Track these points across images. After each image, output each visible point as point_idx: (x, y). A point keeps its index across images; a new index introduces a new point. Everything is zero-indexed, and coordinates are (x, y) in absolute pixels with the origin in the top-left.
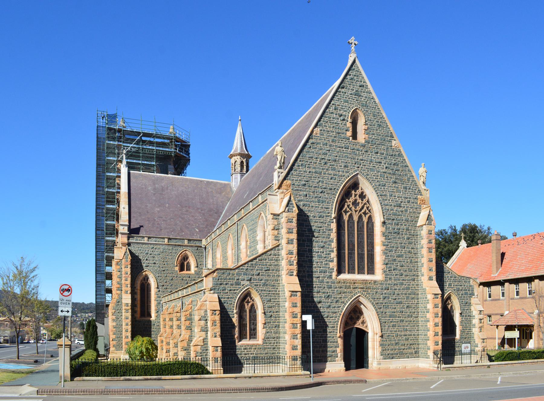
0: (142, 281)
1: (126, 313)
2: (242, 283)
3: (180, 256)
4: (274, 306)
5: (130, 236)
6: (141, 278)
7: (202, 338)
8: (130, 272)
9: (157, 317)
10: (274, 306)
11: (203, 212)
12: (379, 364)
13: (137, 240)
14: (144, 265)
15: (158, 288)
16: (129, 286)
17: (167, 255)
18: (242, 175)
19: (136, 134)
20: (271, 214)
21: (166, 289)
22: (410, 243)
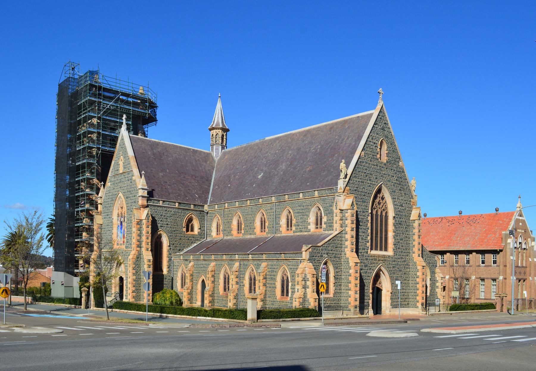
0: (156, 239)
2: (324, 255)
4: (339, 272)
6: (156, 237)
7: (303, 293)
10: (339, 272)
11: (196, 178)
12: (390, 311)
13: (154, 203)
14: (159, 225)
15: (169, 246)
16: (150, 244)
19: (115, 92)
20: (339, 209)
22: (407, 231)
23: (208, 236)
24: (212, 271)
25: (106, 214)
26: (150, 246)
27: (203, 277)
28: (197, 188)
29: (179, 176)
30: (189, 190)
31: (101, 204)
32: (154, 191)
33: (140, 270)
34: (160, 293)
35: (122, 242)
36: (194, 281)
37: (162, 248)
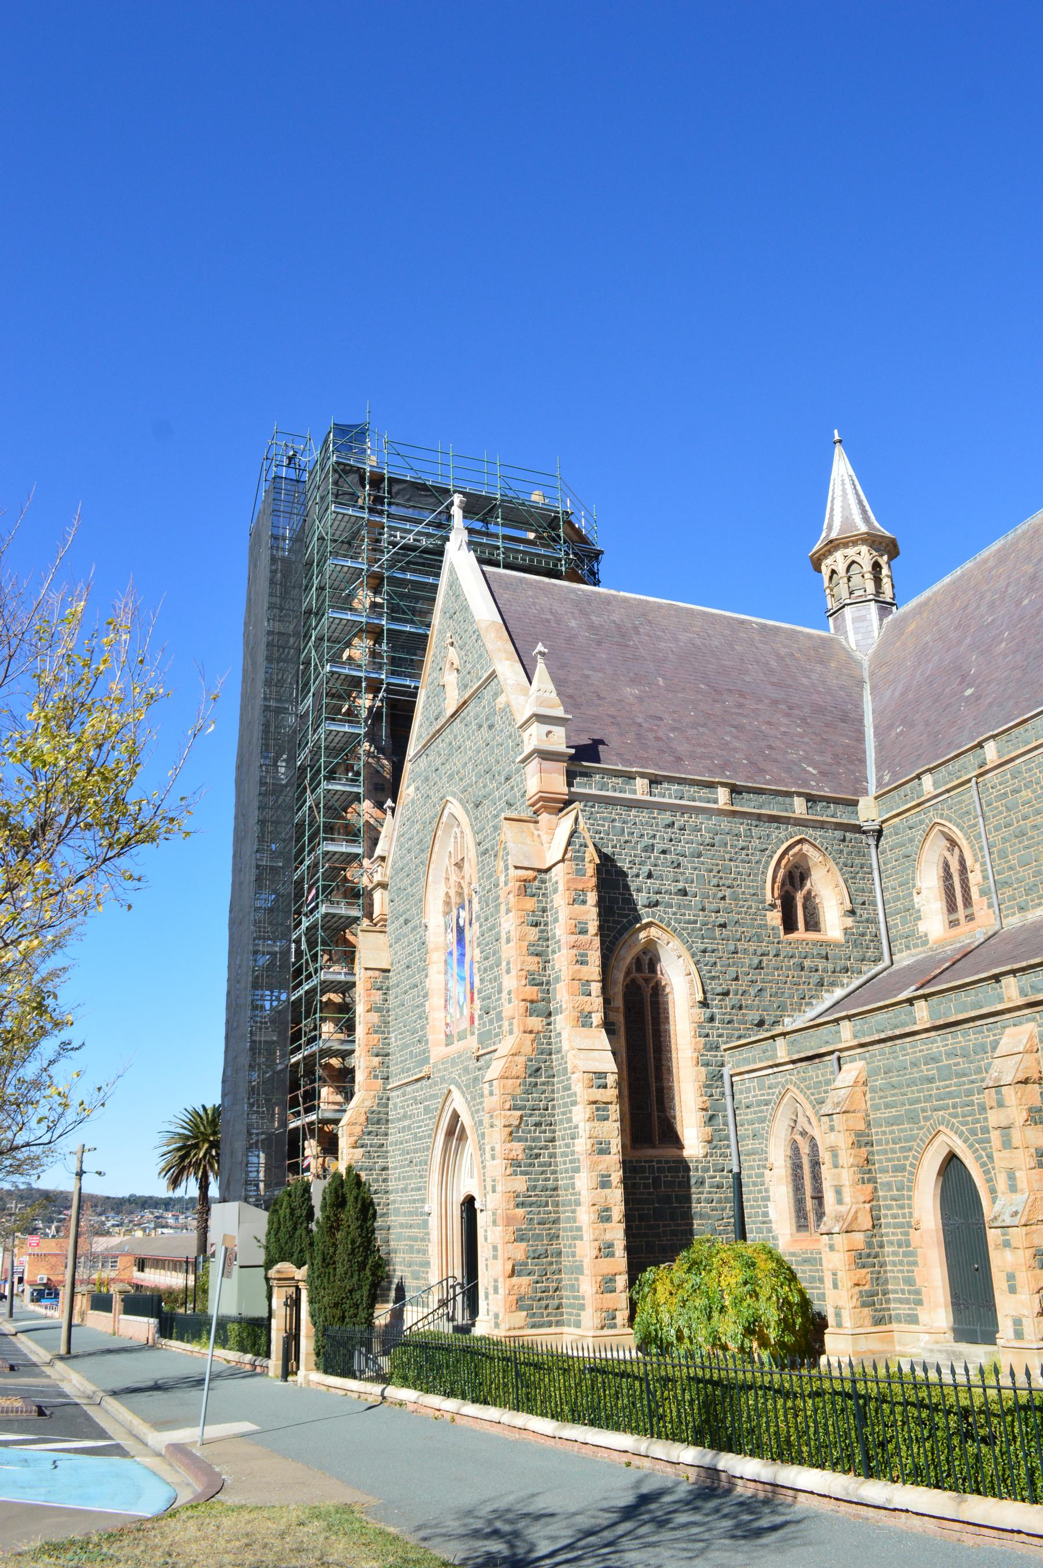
0: (628, 972)
1: (596, 1124)
3: (784, 862)
5: (573, 768)
8: (597, 923)
9: (709, 1142)
11: (796, 712)
13: (603, 787)
14: (640, 899)
15: (704, 1004)
16: (596, 988)
17: (731, 860)
18: (885, 607)
21: (740, 1008)
23: (897, 945)
24: (1026, 1082)
25: (402, 920)
26: (596, 1002)
27: (951, 1141)
28: (807, 743)
29: (715, 701)
30: (770, 747)
31: (383, 886)
32: (601, 747)
33: (553, 1140)
34: (678, 1268)
35: (465, 1024)
36: (882, 1178)
37: (667, 1018)
